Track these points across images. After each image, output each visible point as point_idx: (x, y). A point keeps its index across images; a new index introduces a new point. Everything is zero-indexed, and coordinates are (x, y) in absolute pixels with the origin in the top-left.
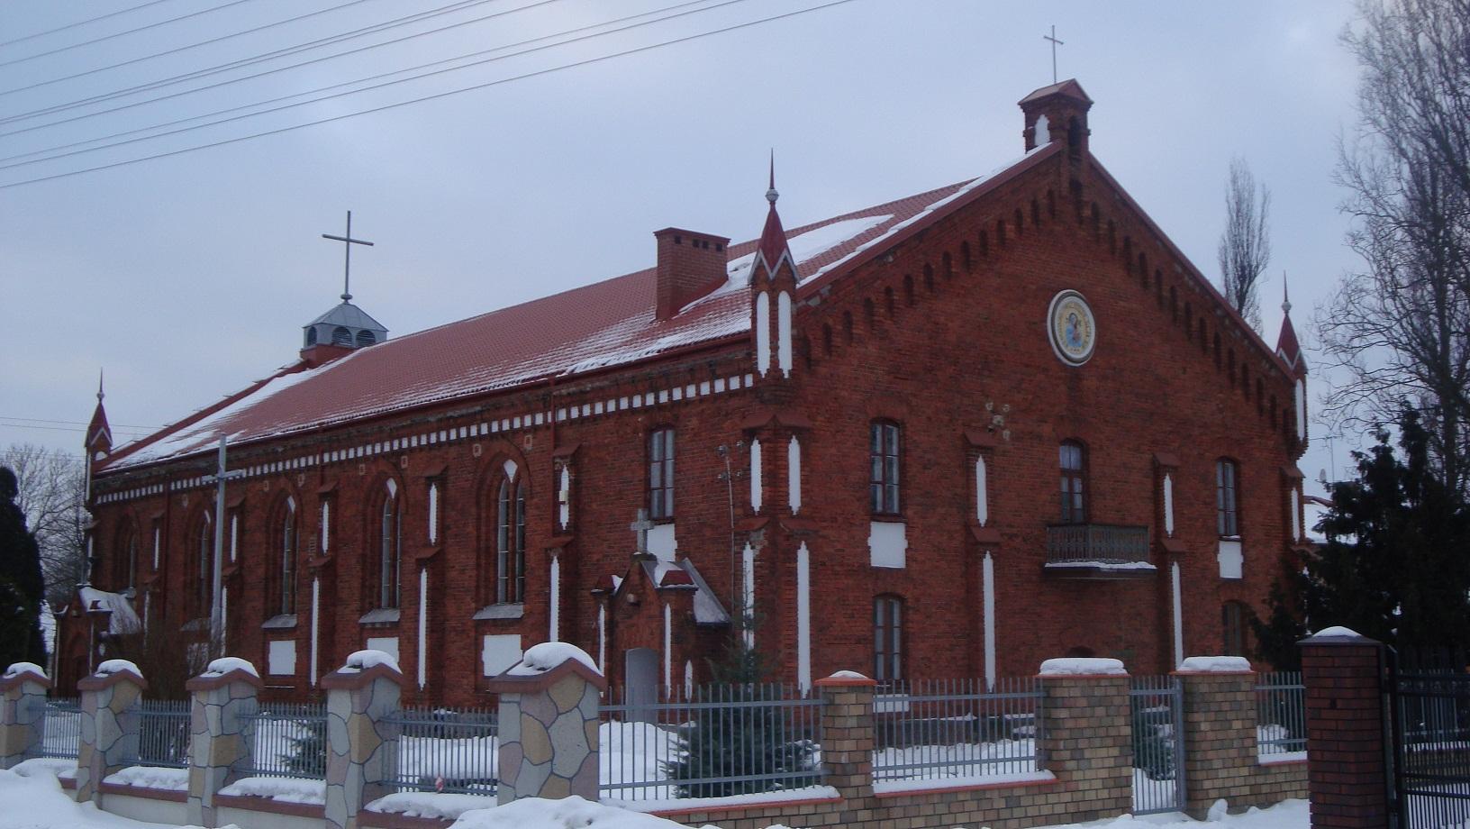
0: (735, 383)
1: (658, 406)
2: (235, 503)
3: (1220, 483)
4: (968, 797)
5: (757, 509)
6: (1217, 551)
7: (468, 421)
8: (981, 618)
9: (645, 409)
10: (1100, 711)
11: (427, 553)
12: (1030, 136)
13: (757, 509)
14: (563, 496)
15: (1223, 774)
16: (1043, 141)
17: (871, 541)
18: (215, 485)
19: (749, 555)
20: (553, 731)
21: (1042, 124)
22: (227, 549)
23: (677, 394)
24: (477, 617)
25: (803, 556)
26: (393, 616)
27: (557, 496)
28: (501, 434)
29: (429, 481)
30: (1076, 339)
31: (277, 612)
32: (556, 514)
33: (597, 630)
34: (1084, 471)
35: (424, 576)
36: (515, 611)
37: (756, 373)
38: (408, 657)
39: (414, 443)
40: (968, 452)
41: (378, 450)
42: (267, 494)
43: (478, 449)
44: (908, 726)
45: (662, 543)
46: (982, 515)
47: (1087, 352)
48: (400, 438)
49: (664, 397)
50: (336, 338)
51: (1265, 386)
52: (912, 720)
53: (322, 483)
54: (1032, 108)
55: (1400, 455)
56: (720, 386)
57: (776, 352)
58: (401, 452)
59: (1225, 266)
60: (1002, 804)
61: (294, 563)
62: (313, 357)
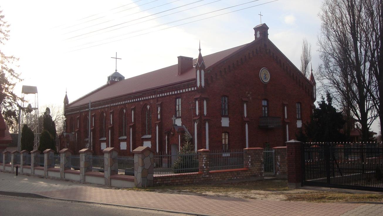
0: (193, 89)
1: (177, 94)
2: (93, 114)
3: (297, 108)
4: (229, 172)
5: (197, 115)
6: (296, 122)
7: (139, 97)
8: (245, 136)
9: (175, 94)
10: (257, 156)
11: (132, 124)
12: (256, 35)
13: (197, 115)
14: (159, 112)
15: (283, 168)
16: (258, 36)
17: (222, 121)
18: (88, 111)
19: (196, 124)
20: (144, 160)
21: (258, 33)
22: (92, 124)
23: (181, 91)
24: (142, 138)
25: (207, 125)
26: (125, 137)
27: (157, 112)
28: (146, 100)
29: (132, 109)
30: (266, 78)
31: (102, 137)
32: (157, 116)
33: (166, 140)
34: (268, 106)
35: (131, 129)
36: (150, 136)
37: (197, 87)
38: (154, 144)
39: (136, 100)
40: (243, 102)
41: (121, 103)
42: (100, 112)
43: (106, 109)
44: (226, 159)
45: (178, 122)
46: (245, 115)
47: (268, 81)
48: (126, 101)
49: (179, 92)
50: (115, 79)
51: (307, 87)
52: (230, 158)
53: (110, 110)
54: (256, 29)
55: (327, 102)
56: (190, 90)
57: (200, 82)
58: (126, 103)
59: (302, 61)
60: (236, 174)
61: (105, 127)
62: (109, 83)
